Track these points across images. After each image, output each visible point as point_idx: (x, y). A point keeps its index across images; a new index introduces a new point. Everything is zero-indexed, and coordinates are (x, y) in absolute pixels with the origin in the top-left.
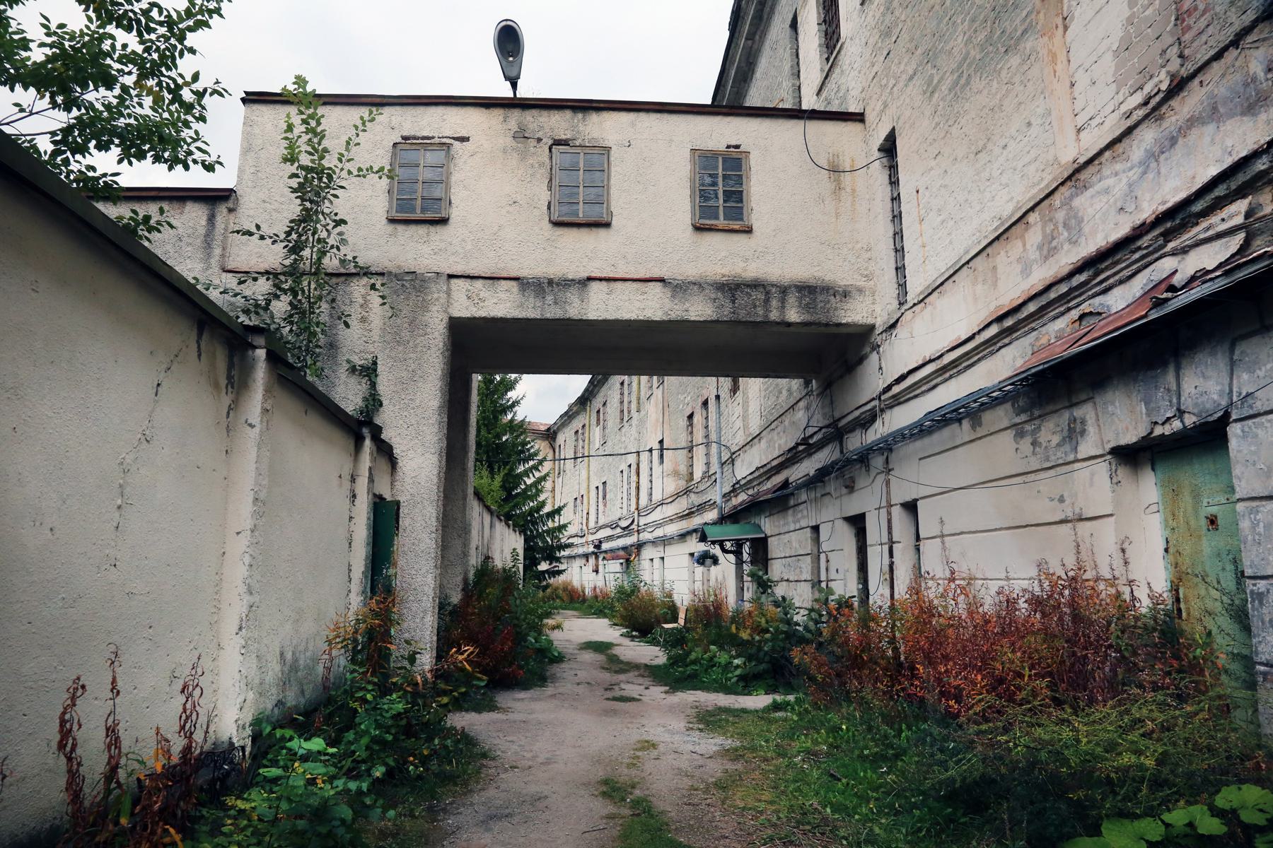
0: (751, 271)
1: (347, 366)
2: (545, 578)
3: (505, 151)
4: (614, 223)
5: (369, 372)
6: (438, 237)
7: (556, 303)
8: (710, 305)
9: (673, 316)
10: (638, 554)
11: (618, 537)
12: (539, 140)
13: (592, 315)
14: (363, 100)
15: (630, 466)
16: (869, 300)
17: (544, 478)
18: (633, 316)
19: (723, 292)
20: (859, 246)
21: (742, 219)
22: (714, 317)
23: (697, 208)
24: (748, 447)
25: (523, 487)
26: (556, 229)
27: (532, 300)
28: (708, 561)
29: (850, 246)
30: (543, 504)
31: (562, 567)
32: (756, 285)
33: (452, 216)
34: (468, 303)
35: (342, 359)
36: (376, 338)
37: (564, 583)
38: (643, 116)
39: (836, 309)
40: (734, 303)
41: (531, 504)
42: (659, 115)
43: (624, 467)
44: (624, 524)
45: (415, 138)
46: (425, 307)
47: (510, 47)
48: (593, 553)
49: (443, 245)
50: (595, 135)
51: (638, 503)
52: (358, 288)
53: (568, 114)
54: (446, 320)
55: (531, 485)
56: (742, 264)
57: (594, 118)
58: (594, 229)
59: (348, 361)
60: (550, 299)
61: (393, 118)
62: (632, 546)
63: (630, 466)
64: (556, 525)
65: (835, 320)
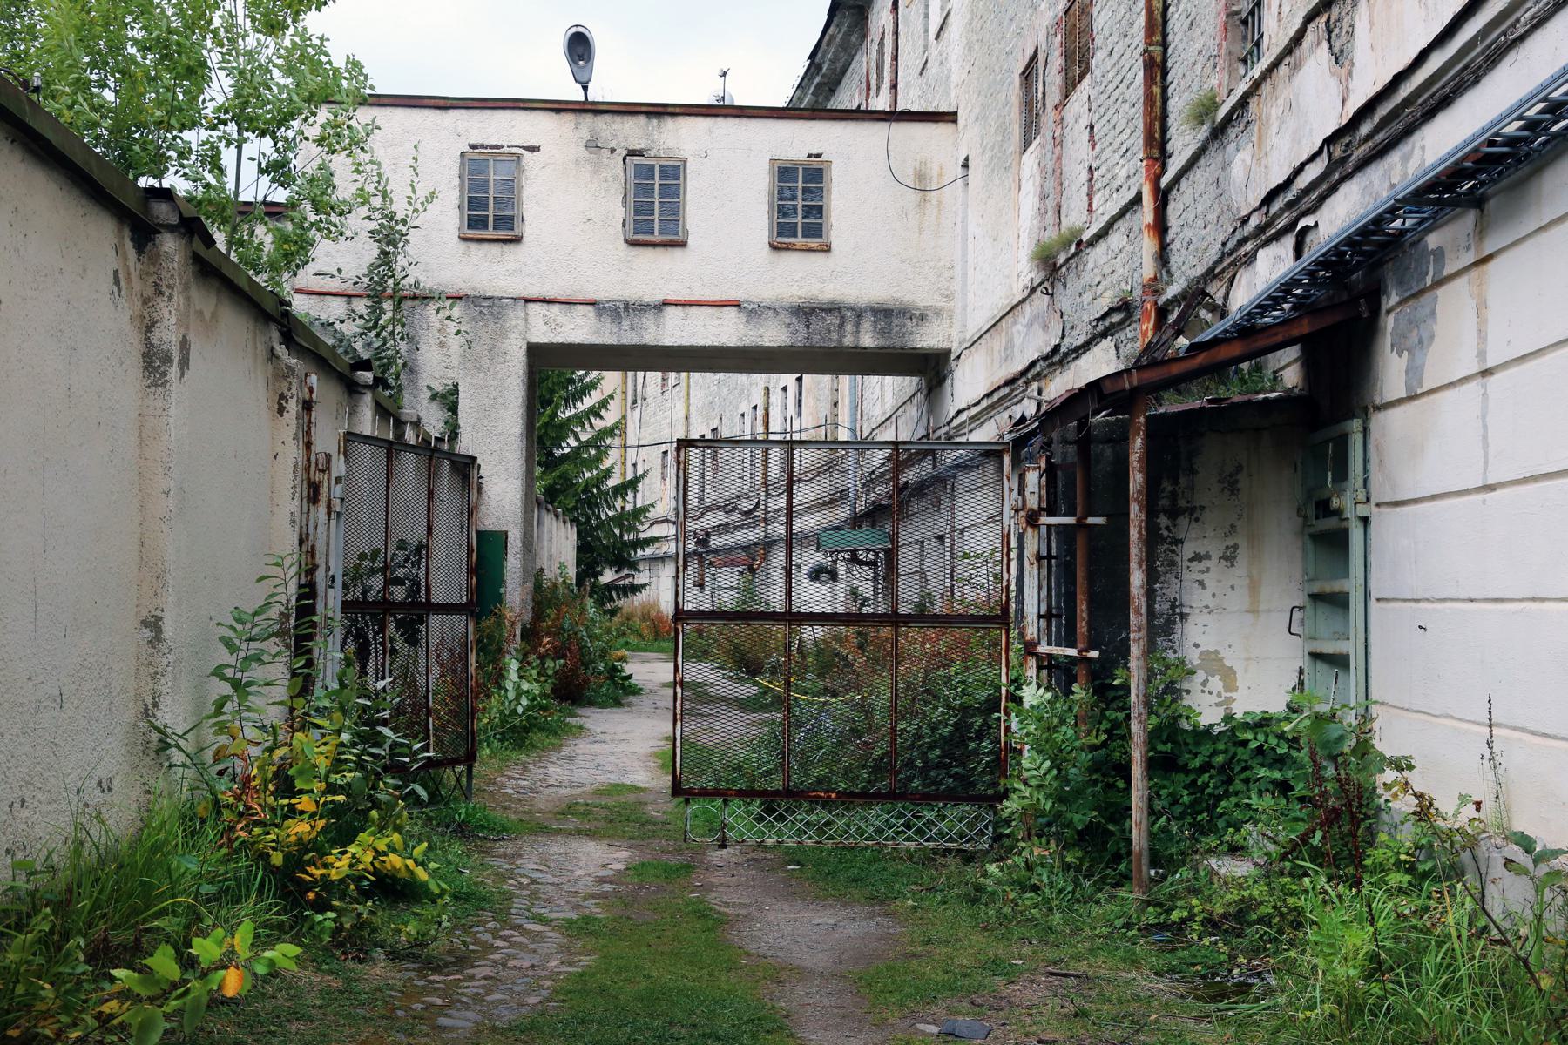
1: (428, 394)
2: (611, 599)
3: (577, 162)
4: (690, 242)
5: (449, 400)
7: (632, 329)
8: (784, 330)
9: (748, 342)
10: (765, 559)
11: (737, 528)
12: (613, 150)
13: (668, 341)
14: (427, 102)
15: (755, 408)
16: (946, 323)
17: (610, 432)
18: (707, 342)
20: (942, 263)
21: (821, 236)
23: (775, 225)
24: (881, 428)
25: (573, 443)
26: (631, 248)
27: (608, 325)
28: (824, 576)
29: (932, 264)
30: (608, 473)
31: (640, 579)
32: (834, 308)
33: (525, 235)
34: (546, 328)
35: (423, 384)
36: (456, 364)
37: (643, 606)
38: (720, 121)
39: (911, 333)
40: (808, 327)
41: (588, 475)
42: (737, 121)
44: (746, 506)
45: (483, 147)
46: (503, 334)
47: (580, 50)
48: (695, 553)
50: (670, 144)
51: (765, 474)
53: (642, 119)
54: (524, 347)
55: (588, 444)
56: (819, 286)
57: (670, 124)
58: (670, 249)
59: (429, 387)
60: (626, 324)
61: (459, 123)
62: (756, 544)
63: (755, 408)
64: (629, 507)
65: (910, 345)
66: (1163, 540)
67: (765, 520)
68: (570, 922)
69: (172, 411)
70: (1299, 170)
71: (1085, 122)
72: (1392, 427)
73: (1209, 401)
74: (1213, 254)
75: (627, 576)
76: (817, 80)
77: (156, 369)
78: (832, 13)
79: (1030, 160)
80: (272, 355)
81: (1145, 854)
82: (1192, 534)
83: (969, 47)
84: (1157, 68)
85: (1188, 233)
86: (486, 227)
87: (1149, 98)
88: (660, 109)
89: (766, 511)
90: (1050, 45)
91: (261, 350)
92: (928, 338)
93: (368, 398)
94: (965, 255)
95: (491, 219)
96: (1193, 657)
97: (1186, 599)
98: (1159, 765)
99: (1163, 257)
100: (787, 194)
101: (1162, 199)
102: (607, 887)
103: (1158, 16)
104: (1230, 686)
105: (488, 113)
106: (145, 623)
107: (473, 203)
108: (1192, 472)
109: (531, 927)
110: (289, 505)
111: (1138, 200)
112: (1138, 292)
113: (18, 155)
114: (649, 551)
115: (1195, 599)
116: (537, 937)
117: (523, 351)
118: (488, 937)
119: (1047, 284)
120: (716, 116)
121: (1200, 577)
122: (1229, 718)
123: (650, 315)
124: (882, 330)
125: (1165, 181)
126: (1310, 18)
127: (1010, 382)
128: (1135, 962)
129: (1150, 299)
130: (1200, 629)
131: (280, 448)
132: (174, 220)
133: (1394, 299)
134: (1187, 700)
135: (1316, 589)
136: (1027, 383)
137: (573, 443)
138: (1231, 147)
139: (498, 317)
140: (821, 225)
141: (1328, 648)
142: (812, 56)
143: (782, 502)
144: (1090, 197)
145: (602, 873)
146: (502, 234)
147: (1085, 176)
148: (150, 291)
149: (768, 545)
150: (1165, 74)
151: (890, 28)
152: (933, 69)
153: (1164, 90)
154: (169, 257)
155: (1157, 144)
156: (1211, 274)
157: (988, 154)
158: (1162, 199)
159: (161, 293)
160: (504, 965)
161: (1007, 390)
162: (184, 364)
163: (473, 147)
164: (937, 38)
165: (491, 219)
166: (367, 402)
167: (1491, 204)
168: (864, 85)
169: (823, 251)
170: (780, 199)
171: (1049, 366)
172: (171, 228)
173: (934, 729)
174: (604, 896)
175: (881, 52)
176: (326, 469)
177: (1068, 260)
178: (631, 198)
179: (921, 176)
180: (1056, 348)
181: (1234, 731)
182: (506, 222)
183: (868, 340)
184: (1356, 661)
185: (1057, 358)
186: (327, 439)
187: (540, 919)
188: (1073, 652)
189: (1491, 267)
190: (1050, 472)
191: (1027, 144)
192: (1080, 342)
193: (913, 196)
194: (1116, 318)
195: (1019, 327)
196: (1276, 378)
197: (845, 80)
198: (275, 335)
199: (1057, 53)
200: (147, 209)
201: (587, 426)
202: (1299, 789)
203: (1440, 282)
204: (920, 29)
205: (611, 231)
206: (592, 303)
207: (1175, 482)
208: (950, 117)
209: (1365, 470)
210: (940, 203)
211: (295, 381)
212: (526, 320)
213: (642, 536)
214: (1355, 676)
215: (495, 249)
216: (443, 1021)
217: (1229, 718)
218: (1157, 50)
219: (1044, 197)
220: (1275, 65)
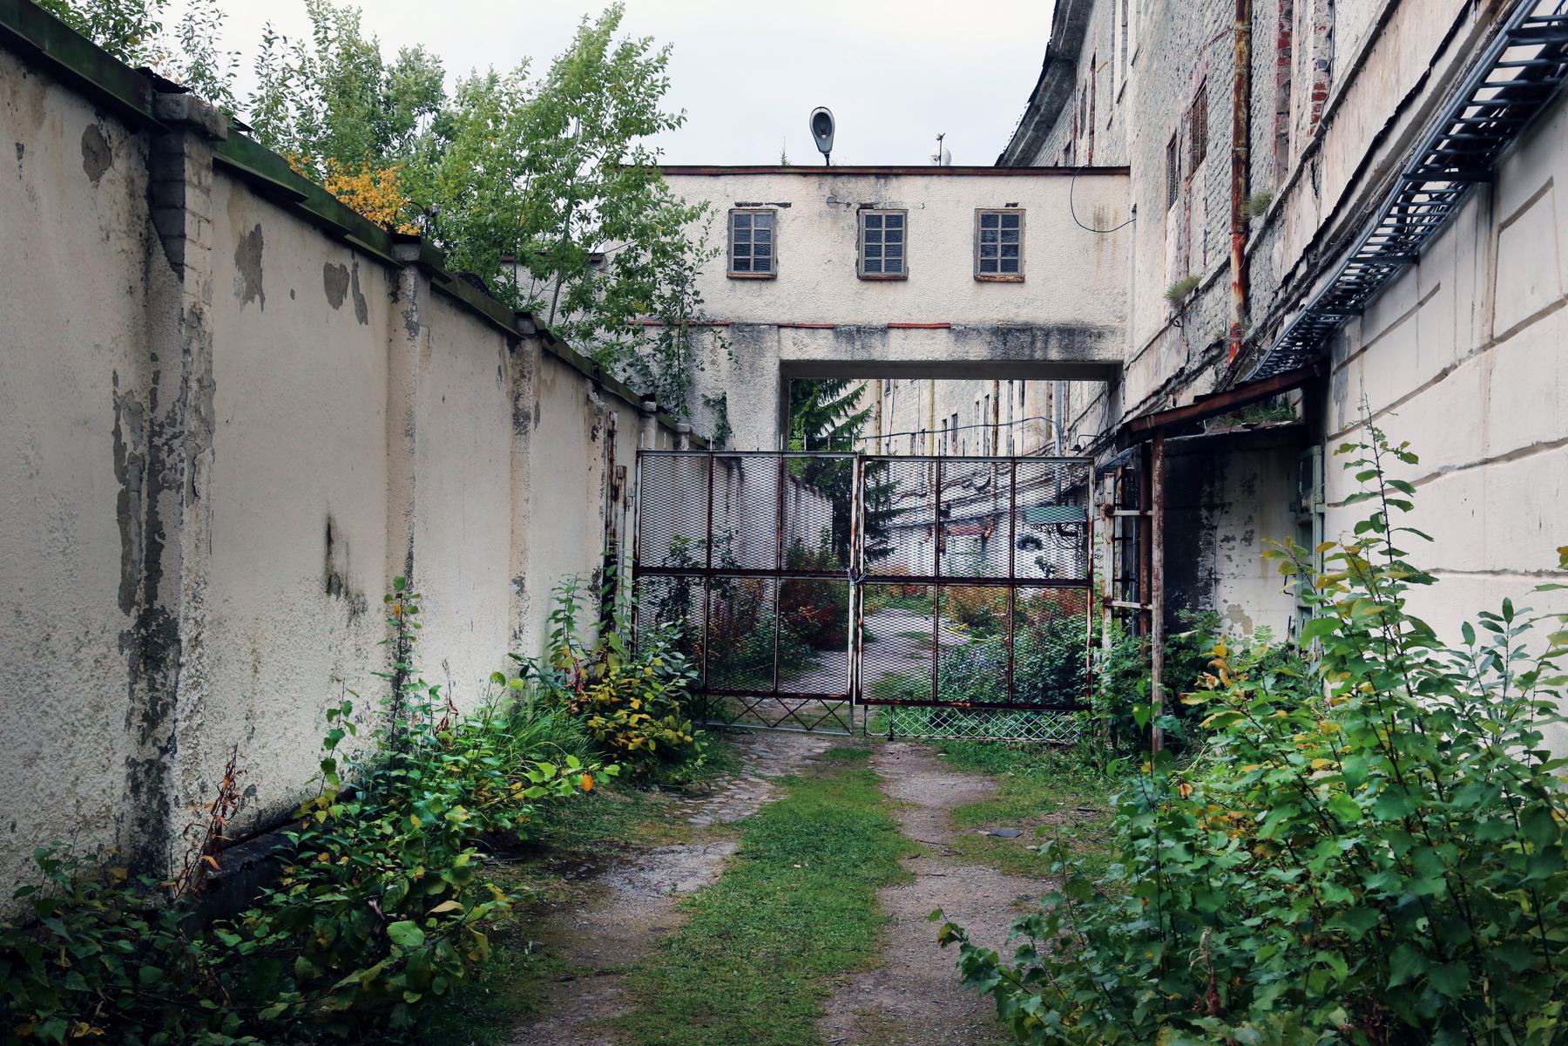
0: (1024, 315)
3: (820, 215)
6: (768, 292)
9: (956, 357)
11: (973, 501)
12: (849, 205)
13: (892, 357)
15: (988, 397)
16: (1119, 340)
17: (862, 418)
18: (924, 358)
19: (997, 336)
22: (989, 357)
32: (1027, 329)
34: (794, 348)
35: (698, 393)
38: (935, 179)
42: (949, 178)
43: (980, 397)
44: (980, 482)
45: (748, 205)
47: (823, 126)
49: (772, 299)
52: (707, 338)
53: (872, 180)
55: (842, 428)
57: (894, 182)
60: (858, 344)
63: (988, 397)
65: (1089, 358)
66: (1204, 527)
67: (995, 495)
68: (778, 778)
69: (531, 450)
73: (1245, 427)
75: (879, 544)
76: (1037, 118)
77: (521, 424)
80: (588, 400)
81: (1160, 740)
82: (1223, 523)
83: (1138, 115)
84: (1242, 164)
86: (748, 268)
87: (1236, 187)
88: (887, 171)
89: (996, 487)
90: (1183, 128)
91: (582, 397)
92: (1105, 352)
93: (653, 421)
94: (1133, 285)
95: (752, 262)
96: (1223, 609)
97: (1218, 568)
100: (989, 236)
102: (808, 762)
103: (1243, 125)
105: (750, 179)
106: (515, 582)
107: (740, 249)
108: (1223, 479)
109: (753, 779)
110: (600, 502)
111: (1227, 264)
113: (453, 311)
114: (897, 520)
115: (1225, 568)
116: (756, 785)
117: (777, 367)
118: (725, 784)
119: (1179, 319)
120: (932, 175)
121: (1228, 553)
123: (877, 336)
124: (1066, 345)
130: (1228, 590)
131: (593, 463)
132: (532, 331)
136: (1167, 395)
137: (831, 429)
140: (1016, 261)
142: (1032, 99)
143: (1007, 480)
144: (1205, 252)
145: (807, 754)
146: (761, 274)
148: (518, 376)
149: (996, 516)
151: (1089, 83)
153: (1248, 180)
154: (529, 354)
155: (1241, 227)
157: (1148, 205)
158: (1245, 263)
159: (524, 376)
160: (732, 797)
161: (1153, 400)
162: (537, 419)
163: (738, 205)
164: (1118, 102)
165: (752, 262)
166: (652, 423)
167: (1367, 314)
169: (1018, 282)
170: (983, 241)
171: (1180, 383)
172: (530, 336)
173: (1052, 662)
174: (807, 766)
175: (1084, 101)
176: (623, 477)
177: (1191, 301)
178: (863, 243)
179: (1099, 220)
180: (1182, 370)
183: (1054, 354)
185: (1183, 378)
186: (625, 456)
187: (760, 777)
188: (1137, 606)
192: (1195, 367)
194: (1214, 352)
195: (1163, 349)
197: (1060, 119)
198: (590, 385)
199: (1187, 137)
200: (516, 326)
201: (842, 413)
204: (1108, 88)
205: (847, 269)
206: (832, 328)
207: (1212, 486)
208: (1124, 171)
209: (1323, 481)
210: (1115, 241)
211: (603, 418)
212: (779, 342)
213: (894, 507)
215: (755, 286)
216: (691, 820)
218: (1242, 150)
219: (1179, 248)
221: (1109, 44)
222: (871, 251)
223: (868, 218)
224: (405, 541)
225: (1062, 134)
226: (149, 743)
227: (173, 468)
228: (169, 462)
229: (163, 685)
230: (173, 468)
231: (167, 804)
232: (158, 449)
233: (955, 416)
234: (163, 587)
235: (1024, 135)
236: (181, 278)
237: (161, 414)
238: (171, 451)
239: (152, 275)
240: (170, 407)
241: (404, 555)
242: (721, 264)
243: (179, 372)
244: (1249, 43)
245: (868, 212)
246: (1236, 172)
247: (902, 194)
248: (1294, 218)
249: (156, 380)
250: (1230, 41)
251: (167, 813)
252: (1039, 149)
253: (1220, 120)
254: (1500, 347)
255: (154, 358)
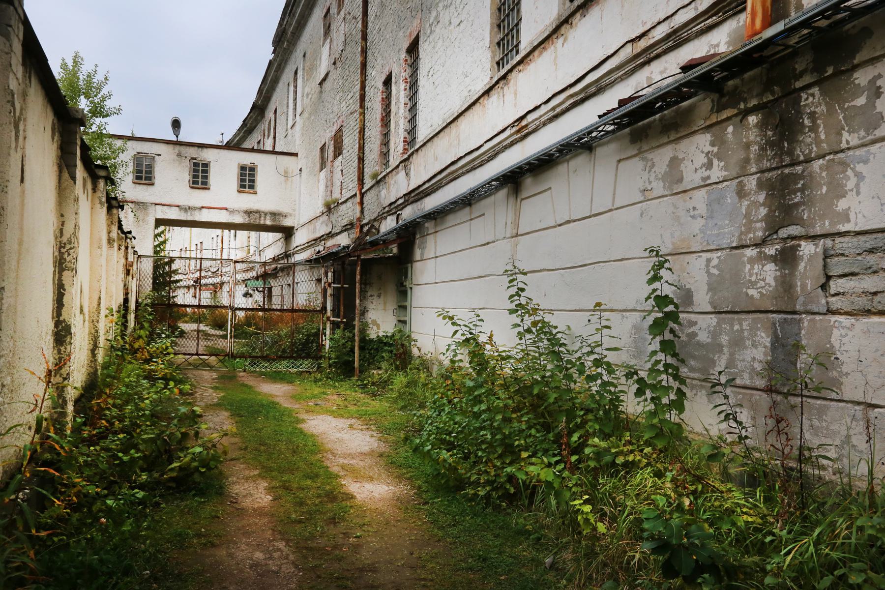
10: (221, 288)
32: (257, 212)
46: (147, 215)
48: (193, 285)
57: (205, 150)
60: (189, 213)
70: (398, 200)
71: (340, 168)
72: (417, 266)
74: (376, 215)
76: (245, 129)
78: (252, 109)
79: (323, 174)
83: (303, 135)
84: (361, 160)
85: (369, 207)
87: (359, 168)
90: (329, 143)
92: (287, 223)
96: (370, 321)
98: (361, 348)
99: (362, 212)
101: (362, 195)
104: (378, 328)
105: (143, 143)
111: (355, 195)
112: (355, 220)
115: (371, 306)
122: (378, 336)
123: (197, 211)
125: (363, 191)
126: (401, 162)
127: (315, 240)
128: (356, 391)
129: (358, 223)
133: (418, 236)
134: (368, 332)
135: (400, 304)
136: (321, 241)
138: (381, 187)
139: (145, 209)
141: (402, 319)
142: (244, 121)
144: (341, 190)
146: (147, 182)
147: (340, 184)
148: (110, 223)
149: (222, 284)
150: (363, 161)
152: (289, 137)
153: (363, 165)
155: (361, 181)
156: (375, 220)
157: (308, 169)
158: (362, 195)
161: (314, 242)
167: (438, 220)
168: (262, 134)
176: (131, 266)
178: (192, 173)
179: (286, 172)
180: (330, 232)
181: (380, 340)
182: (149, 178)
183: (268, 222)
184: (408, 322)
188: (339, 320)
189: (438, 234)
190: (334, 272)
191: (321, 170)
192: (338, 231)
193: (284, 178)
194: (349, 227)
196: (392, 250)
202: (395, 352)
203: (428, 235)
206: (178, 206)
208: (296, 155)
214: (408, 325)
215: (145, 187)
217: (378, 336)
219: (327, 187)
220: (392, 170)
221: (285, 106)
222: (195, 177)
223: (194, 163)
224: (98, 292)
225: (256, 137)
226: (58, 376)
227: (70, 262)
228: (68, 259)
229: (65, 352)
230: (70, 262)
231: (66, 401)
232: (63, 253)
233: (201, 243)
234: (64, 311)
235: (239, 134)
236: (75, 183)
237: (65, 239)
238: (69, 254)
239: (62, 181)
240: (69, 236)
241: (97, 298)
242: (130, 178)
243: (74, 222)
244: (364, 117)
245: (194, 161)
246: (359, 162)
247: (208, 155)
248: (392, 182)
249: (63, 224)
250: (357, 115)
251: (66, 405)
252: (245, 141)
253: (350, 142)
254: (520, 238)
255: (62, 215)
